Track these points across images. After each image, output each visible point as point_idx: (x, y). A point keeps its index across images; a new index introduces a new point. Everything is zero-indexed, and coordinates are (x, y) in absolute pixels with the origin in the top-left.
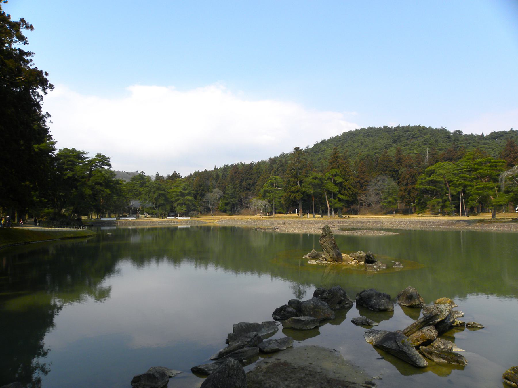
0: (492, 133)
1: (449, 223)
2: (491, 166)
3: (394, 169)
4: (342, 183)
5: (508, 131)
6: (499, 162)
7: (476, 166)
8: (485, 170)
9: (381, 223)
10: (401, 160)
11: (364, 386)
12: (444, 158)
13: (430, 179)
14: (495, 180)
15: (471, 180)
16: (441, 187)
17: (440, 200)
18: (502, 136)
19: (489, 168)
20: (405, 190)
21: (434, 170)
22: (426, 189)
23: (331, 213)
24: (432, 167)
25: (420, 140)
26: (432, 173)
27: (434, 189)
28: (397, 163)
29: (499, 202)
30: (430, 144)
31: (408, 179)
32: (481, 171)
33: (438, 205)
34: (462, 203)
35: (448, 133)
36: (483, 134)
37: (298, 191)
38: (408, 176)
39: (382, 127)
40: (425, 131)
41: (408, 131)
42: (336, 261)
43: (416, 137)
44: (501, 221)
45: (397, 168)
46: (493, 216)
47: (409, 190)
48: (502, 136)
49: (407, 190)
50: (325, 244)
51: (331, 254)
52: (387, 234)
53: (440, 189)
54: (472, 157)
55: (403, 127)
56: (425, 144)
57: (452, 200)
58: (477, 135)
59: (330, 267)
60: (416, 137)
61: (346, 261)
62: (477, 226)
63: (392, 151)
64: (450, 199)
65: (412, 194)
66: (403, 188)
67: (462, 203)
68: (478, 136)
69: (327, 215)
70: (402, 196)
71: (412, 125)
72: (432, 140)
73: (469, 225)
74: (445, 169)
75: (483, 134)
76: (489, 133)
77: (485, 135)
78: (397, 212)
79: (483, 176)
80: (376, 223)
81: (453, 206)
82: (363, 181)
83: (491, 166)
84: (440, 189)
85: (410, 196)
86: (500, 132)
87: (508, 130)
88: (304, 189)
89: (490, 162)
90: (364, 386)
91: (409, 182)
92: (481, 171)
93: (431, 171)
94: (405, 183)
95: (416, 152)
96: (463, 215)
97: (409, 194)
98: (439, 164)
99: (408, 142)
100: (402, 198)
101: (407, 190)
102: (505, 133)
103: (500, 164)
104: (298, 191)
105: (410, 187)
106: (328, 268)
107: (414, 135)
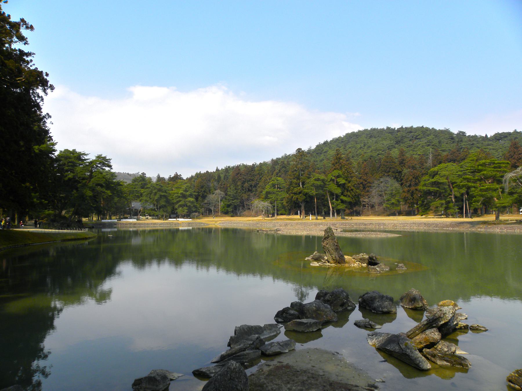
0: (496, 134)
1: (452, 225)
2: (495, 167)
3: (397, 170)
4: (344, 184)
5: (512, 132)
6: (503, 163)
7: (480, 167)
8: (488, 171)
9: (384, 224)
10: (404, 162)
11: (367, 389)
12: (448, 159)
13: (433, 180)
14: (499, 182)
16: (444, 189)
17: (444, 202)
18: (506, 137)
19: (493, 169)
20: (408, 191)
21: (438, 172)
22: (429, 190)
23: (333, 215)
24: (436, 169)
25: (424, 141)
26: (435, 174)
27: (438, 191)
28: (400, 164)
29: (503, 203)
30: (433, 145)
31: (411, 181)
32: (485, 172)
33: (441, 207)
34: (466, 205)
35: (451, 134)
36: (486, 135)
37: (300, 193)
38: (411, 177)
39: (385, 128)
41: (411, 132)
42: (339, 263)
44: (505, 222)
45: (400, 170)
46: (497, 217)
47: (413, 192)
48: (506, 137)
49: (411, 192)
50: (327, 246)
51: (334, 256)
52: (390, 235)
53: (444, 191)
54: (475, 158)
55: (406, 128)
56: (429, 145)
57: (456, 202)
58: (480, 136)
59: (332, 269)
61: (349, 263)
62: (481, 228)
63: (395, 153)
64: (453, 200)
65: (415, 196)
66: (406, 189)
67: (466, 205)
69: (329, 216)
70: (405, 197)
71: (415, 126)
72: (436, 141)
73: (473, 227)
74: (448, 171)
75: (486, 135)
76: (492, 134)
77: (489, 136)
78: (400, 213)
79: (487, 178)
80: (379, 224)
81: (457, 207)
82: (366, 183)
83: (495, 167)
84: (444, 191)
86: (503, 133)
87: (512, 131)
88: (306, 190)
89: (494, 163)
90: (367, 389)
91: (412, 184)
92: (485, 172)
93: (434, 172)
94: (408, 185)
95: (419, 153)
96: (467, 216)
97: (412, 195)
98: (443, 165)
99: (411, 142)
100: (405, 200)
101: (411, 192)
102: (509, 134)
103: (504, 165)
104: (300, 193)
105: (413, 188)
106: (331, 270)
107: (417, 136)
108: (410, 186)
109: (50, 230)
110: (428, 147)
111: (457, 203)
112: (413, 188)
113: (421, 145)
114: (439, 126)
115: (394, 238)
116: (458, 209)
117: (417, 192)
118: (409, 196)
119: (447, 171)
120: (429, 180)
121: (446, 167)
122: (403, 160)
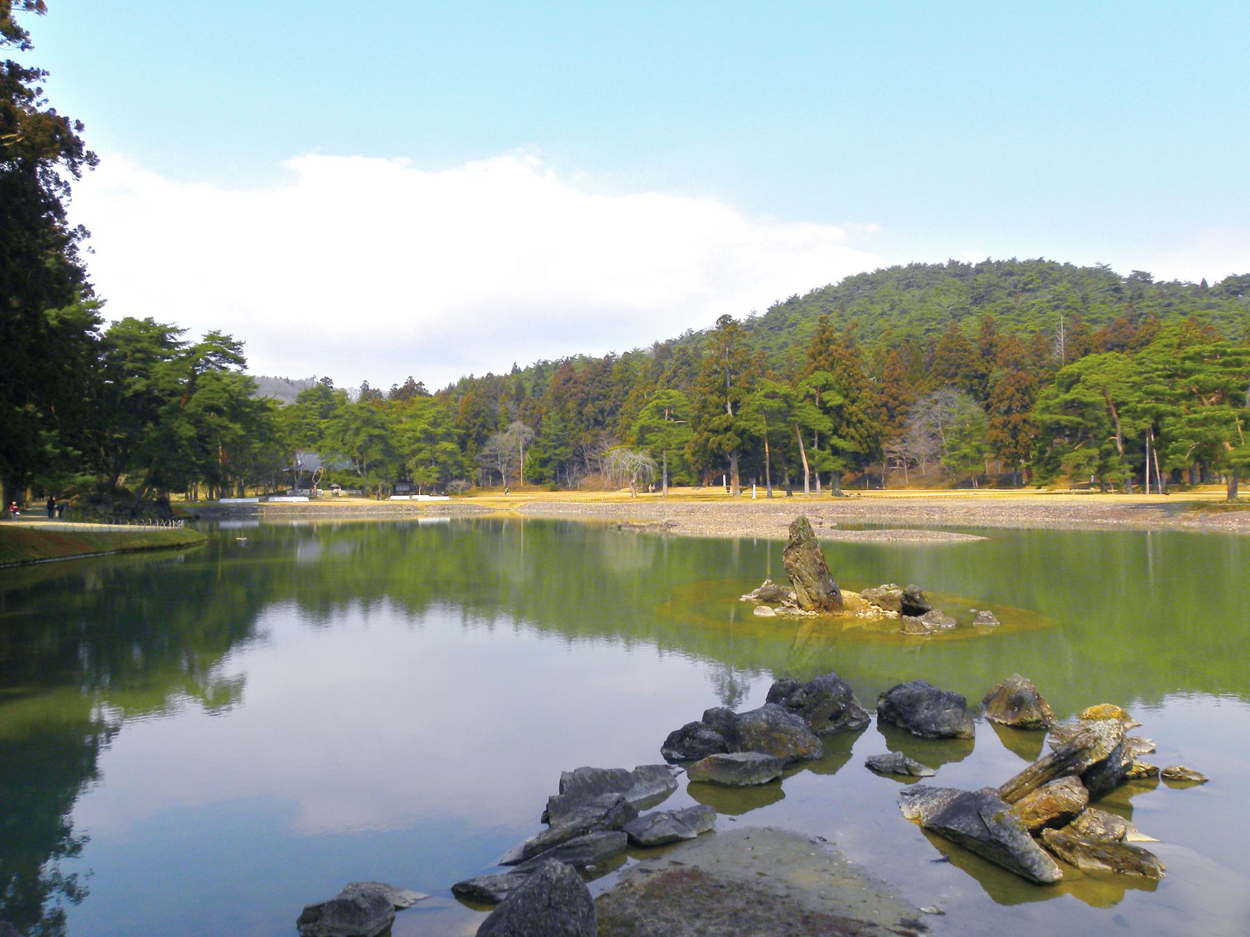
2: (1225, 364)
3: (976, 371)
4: (840, 407)
8: (1209, 374)
9: (942, 510)
10: (994, 349)
12: (1106, 342)
13: (1068, 397)
15: (1175, 401)
16: (1097, 419)
17: (1095, 452)
19: (1221, 369)
20: (1005, 425)
21: (1079, 375)
24: (1074, 368)
27: (1079, 424)
28: (983, 355)
30: (1068, 307)
31: (1011, 398)
32: (1201, 377)
33: (1089, 464)
34: (1152, 460)
36: (1204, 282)
37: (727, 429)
39: (945, 264)
40: (1056, 275)
41: (1011, 274)
43: (1032, 290)
45: (982, 370)
46: (1232, 492)
49: (1010, 426)
50: (797, 565)
51: (813, 592)
53: (1095, 424)
54: (1176, 340)
56: (1056, 307)
57: (1126, 452)
59: (810, 624)
60: (1032, 290)
62: (1191, 519)
63: (970, 327)
64: (1120, 448)
66: (998, 420)
67: (1152, 460)
68: (1192, 287)
72: (1074, 297)
75: (1204, 282)
77: (1210, 285)
83: (1225, 364)
84: (1095, 424)
85: (1017, 442)
89: (1223, 354)
91: (1014, 406)
92: (1201, 377)
93: (1071, 375)
94: (1003, 408)
95: (1032, 327)
97: (1014, 436)
98: (1092, 358)
99: (1011, 300)
100: (997, 446)
101: (1010, 426)
104: (727, 429)
105: (1016, 418)
107: (1026, 284)
108: (1008, 411)
109: (88, 525)
110: (1056, 313)
111: (1129, 456)
112: (1016, 418)
113: (1036, 307)
114: (1083, 260)
115: (982, 541)
116: (1132, 471)
117: (1027, 427)
118: (1006, 437)
119: (1104, 372)
120: (1057, 396)
121: (1099, 364)
122: (991, 345)
